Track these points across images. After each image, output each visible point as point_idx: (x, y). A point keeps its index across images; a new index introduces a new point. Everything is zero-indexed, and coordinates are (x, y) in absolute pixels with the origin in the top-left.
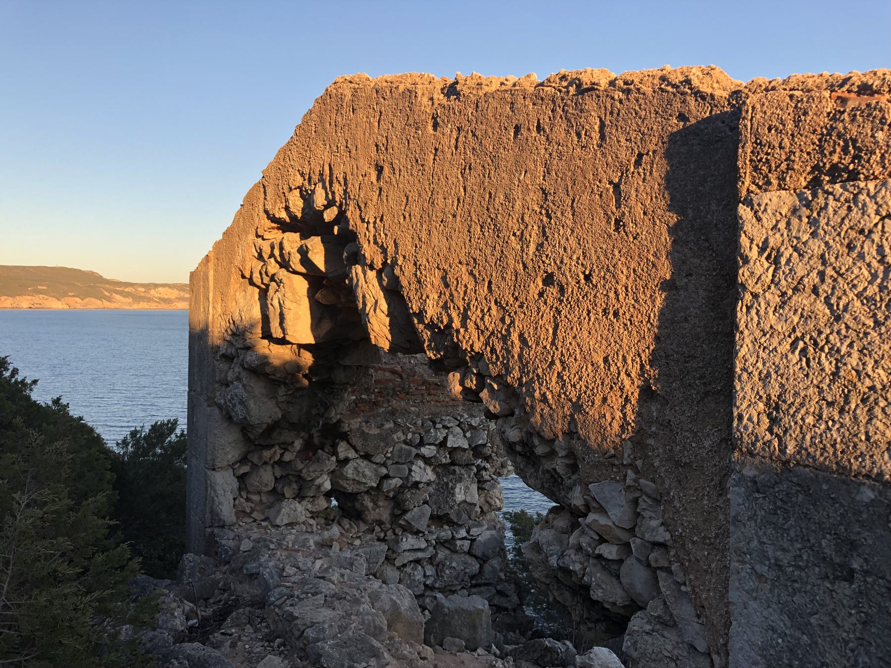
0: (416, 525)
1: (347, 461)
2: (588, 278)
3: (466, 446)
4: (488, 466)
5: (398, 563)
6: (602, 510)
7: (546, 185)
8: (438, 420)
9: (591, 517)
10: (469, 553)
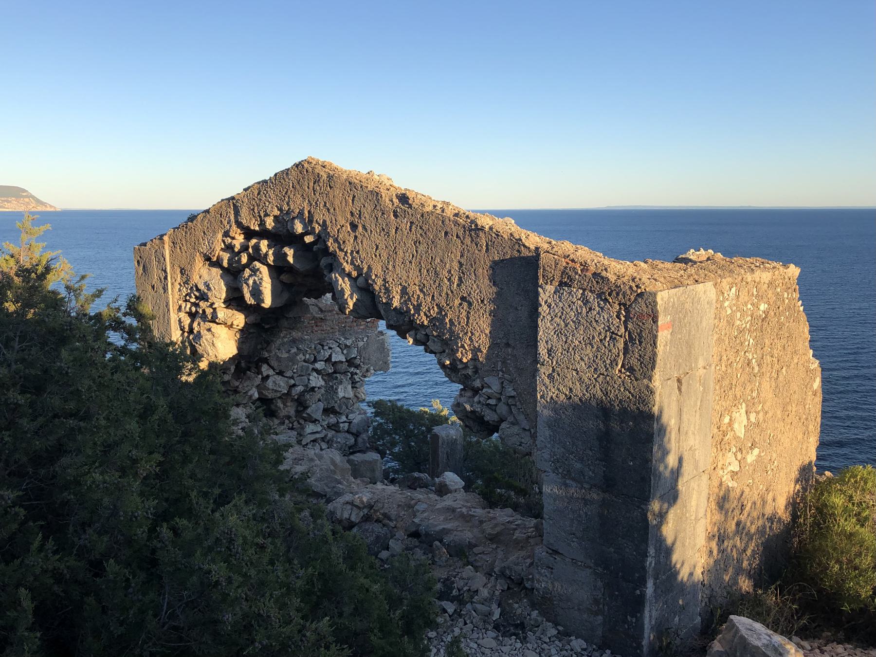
0: (315, 416)
1: (268, 377)
2: (482, 301)
3: (344, 360)
4: (358, 371)
5: (304, 443)
6: (489, 387)
7: (462, 261)
8: (325, 344)
9: (484, 390)
10: (348, 432)
